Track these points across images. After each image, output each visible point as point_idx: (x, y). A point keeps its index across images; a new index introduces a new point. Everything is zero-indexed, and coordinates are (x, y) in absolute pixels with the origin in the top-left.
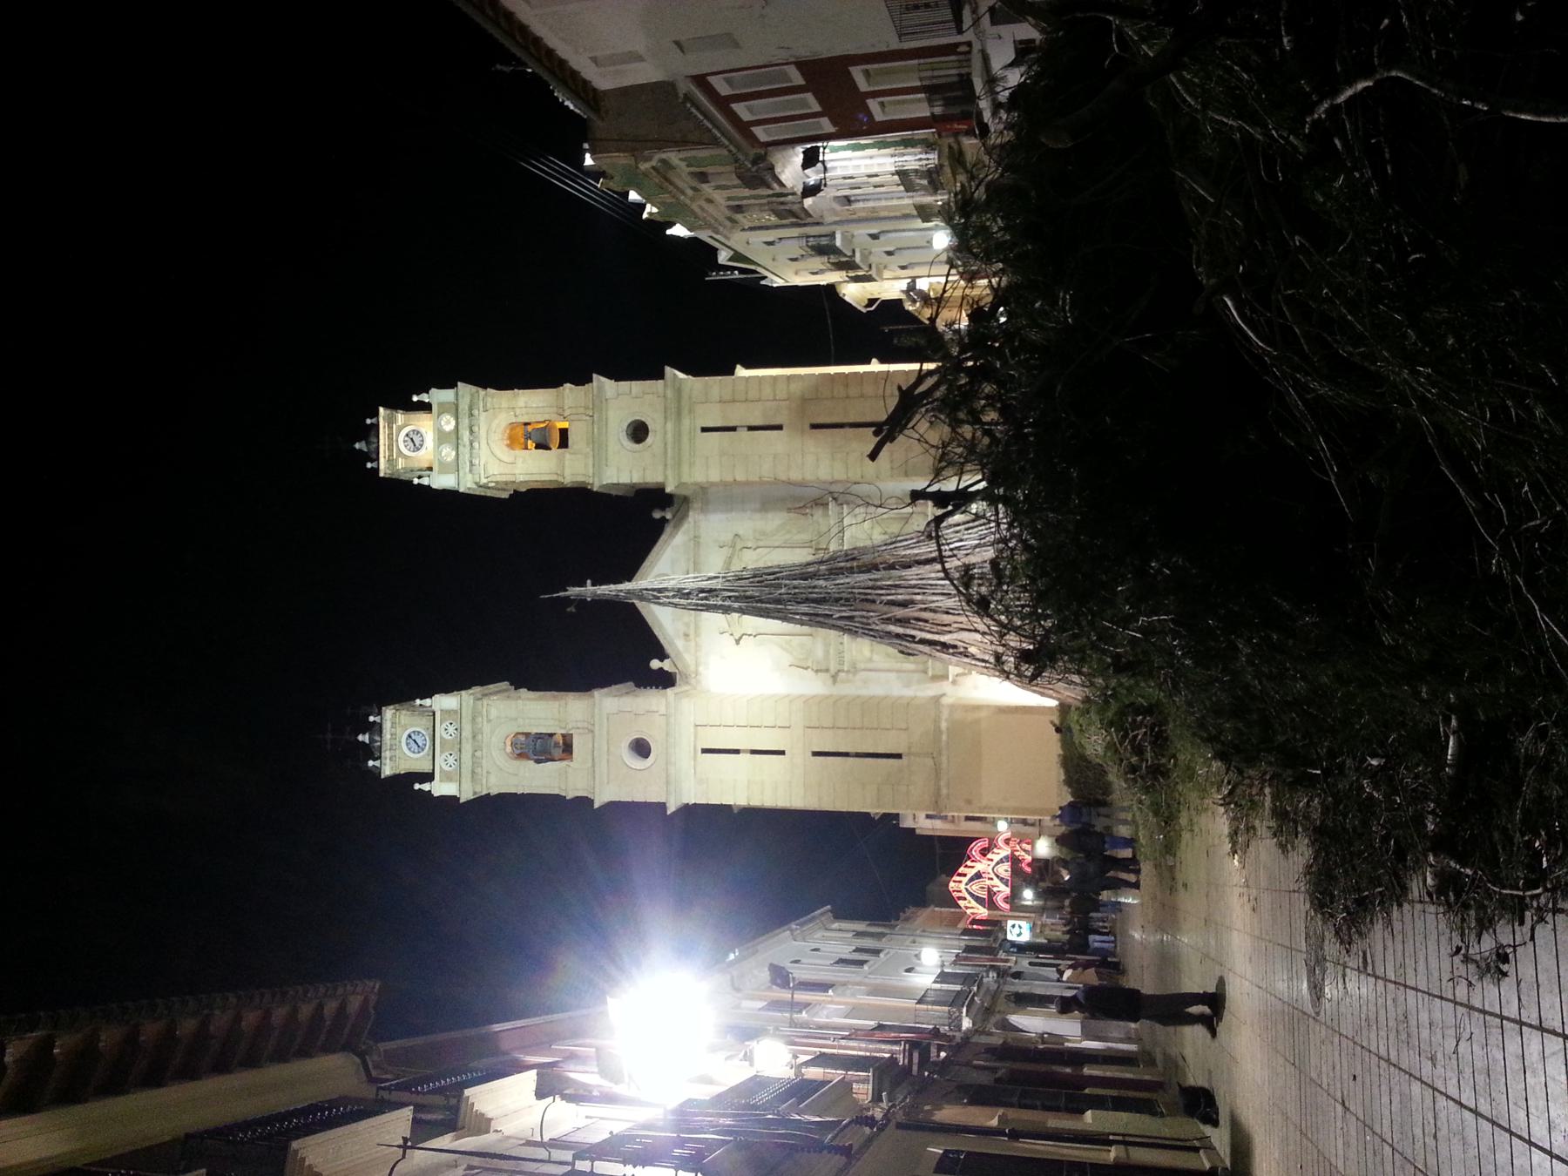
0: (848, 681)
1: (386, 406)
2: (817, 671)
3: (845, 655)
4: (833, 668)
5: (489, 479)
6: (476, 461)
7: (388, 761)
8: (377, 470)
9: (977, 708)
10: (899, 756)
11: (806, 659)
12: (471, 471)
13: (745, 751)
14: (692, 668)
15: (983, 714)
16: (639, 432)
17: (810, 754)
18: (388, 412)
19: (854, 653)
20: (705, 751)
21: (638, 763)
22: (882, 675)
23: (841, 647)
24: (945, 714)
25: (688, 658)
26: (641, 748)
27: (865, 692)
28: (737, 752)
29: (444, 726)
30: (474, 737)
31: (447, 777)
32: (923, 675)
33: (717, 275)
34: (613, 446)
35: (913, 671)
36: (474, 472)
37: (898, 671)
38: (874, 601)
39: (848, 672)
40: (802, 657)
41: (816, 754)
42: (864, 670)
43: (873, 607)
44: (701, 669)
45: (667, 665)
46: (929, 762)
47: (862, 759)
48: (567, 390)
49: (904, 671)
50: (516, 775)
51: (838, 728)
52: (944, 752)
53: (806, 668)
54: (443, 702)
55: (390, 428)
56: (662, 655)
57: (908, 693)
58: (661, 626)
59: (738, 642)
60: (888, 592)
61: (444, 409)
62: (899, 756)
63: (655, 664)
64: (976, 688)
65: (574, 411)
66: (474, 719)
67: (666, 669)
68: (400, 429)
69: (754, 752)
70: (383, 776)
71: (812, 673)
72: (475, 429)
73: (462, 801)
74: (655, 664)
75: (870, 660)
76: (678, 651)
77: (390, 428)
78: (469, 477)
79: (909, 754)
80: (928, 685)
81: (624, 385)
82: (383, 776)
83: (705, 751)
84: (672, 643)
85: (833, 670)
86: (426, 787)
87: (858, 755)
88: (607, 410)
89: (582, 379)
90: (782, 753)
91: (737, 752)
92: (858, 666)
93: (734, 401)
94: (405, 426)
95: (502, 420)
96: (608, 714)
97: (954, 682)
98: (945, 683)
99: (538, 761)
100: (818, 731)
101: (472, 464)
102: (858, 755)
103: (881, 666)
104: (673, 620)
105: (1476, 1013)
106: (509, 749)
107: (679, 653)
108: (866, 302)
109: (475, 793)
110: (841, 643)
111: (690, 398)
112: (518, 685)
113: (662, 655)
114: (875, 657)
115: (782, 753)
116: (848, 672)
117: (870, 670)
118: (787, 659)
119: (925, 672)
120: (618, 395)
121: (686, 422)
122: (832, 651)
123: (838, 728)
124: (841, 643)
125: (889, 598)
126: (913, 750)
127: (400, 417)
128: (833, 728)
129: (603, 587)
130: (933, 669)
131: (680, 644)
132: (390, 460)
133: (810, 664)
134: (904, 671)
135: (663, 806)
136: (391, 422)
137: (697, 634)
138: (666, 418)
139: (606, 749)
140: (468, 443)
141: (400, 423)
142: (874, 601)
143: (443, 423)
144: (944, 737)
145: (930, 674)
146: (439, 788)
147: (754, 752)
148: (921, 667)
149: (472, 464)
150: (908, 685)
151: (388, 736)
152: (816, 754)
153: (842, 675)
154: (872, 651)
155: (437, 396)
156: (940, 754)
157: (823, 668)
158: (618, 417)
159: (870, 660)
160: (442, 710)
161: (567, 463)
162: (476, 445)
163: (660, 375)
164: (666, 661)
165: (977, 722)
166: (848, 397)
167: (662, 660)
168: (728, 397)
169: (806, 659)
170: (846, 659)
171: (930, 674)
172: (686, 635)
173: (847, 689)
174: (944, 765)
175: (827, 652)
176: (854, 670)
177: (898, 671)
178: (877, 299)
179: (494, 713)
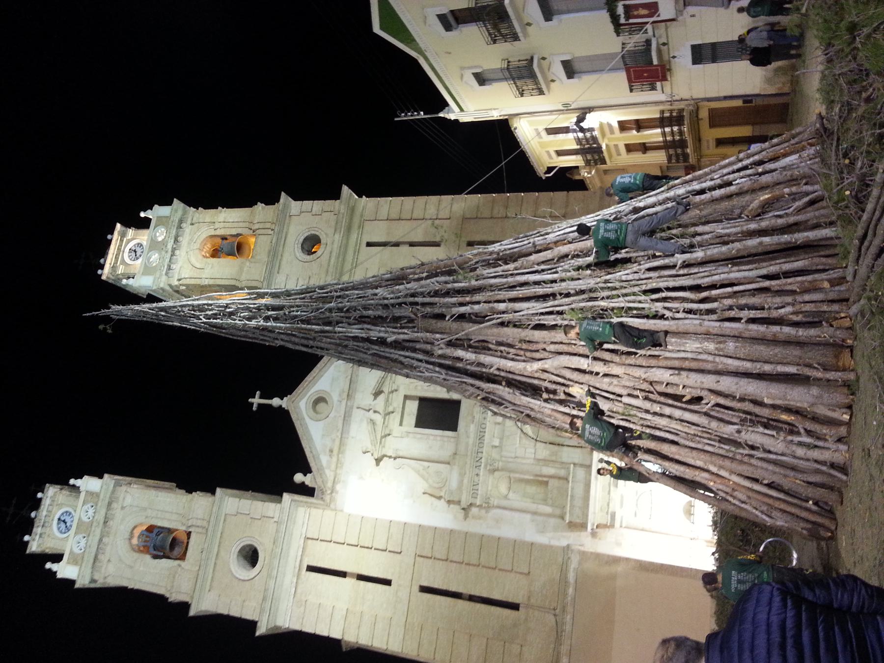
0: (480, 518)
1: (123, 224)
2: (449, 502)
3: (480, 487)
4: (465, 500)
5: (181, 282)
6: (173, 266)
7: (38, 537)
8: (101, 275)
9: (616, 560)
10: (514, 607)
11: (440, 488)
12: (167, 274)
13: (352, 575)
14: (330, 484)
15: (620, 568)
16: (311, 244)
17: (416, 588)
18: (124, 229)
19: (490, 488)
20: (311, 569)
21: (242, 572)
22: (516, 515)
23: (476, 479)
24: (574, 564)
25: (329, 474)
26: (251, 556)
27: (496, 533)
28: (342, 574)
29: (86, 507)
30: (105, 522)
31: (76, 560)
32: (559, 521)
33: (406, 115)
34: (287, 257)
35: (549, 515)
36: (170, 275)
37: (535, 513)
38: (441, 317)
39: (480, 506)
40: (437, 486)
41: (425, 589)
42: (499, 507)
43: (440, 324)
44: (338, 487)
45: (308, 480)
46: (550, 619)
47: (472, 604)
48: (260, 208)
49: (541, 514)
50: (131, 567)
51: (451, 561)
52: (569, 609)
53: (440, 498)
54: (88, 484)
55: (122, 241)
56: (307, 470)
57: (542, 539)
58: (310, 439)
59: (378, 461)
60: (461, 299)
61: (163, 221)
62: (514, 607)
63: (299, 478)
64: (618, 544)
65: (261, 226)
66: (110, 504)
67: (307, 483)
68: (129, 241)
69: (361, 578)
70: (28, 552)
71: (445, 505)
72: (180, 239)
73: (77, 586)
74: (299, 478)
75: (506, 497)
76: (322, 466)
77: (122, 241)
78: (164, 278)
79: (528, 606)
80: (564, 534)
81: (307, 204)
82: (28, 552)
83: (311, 569)
84: (317, 458)
85: (464, 504)
86: (54, 567)
87: (472, 598)
88: (288, 226)
89: (271, 200)
90: (387, 582)
91: (342, 574)
92: (491, 502)
93: (399, 219)
94: (133, 239)
95: (205, 232)
96: (226, 515)
97: (594, 534)
98: (583, 534)
99: (155, 557)
100: (430, 561)
101: (169, 268)
102: (472, 598)
103: (516, 505)
104: (323, 435)
105: (536, 613)
106: (135, 541)
107: (321, 469)
108: (546, 169)
109: (93, 581)
110: (477, 475)
111: (362, 216)
112: (180, 486)
113: (307, 470)
114: (511, 495)
115: (387, 582)
116: (480, 506)
117: (505, 508)
118: (422, 486)
119: (562, 517)
120: (301, 212)
121: (354, 236)
122: (465, 481)
123: (451, 561)
124: (477, 475)
125: (462, 309)
126: (533, 601)
127: (131, 232)
128: (447, 560)
129: (144, 306)
130: (571, 514)
131: (324, 459)
132: (114, 268)
133: (442, 494)
134: (541, 514)
135: (253, 624)
136: (123, 235)
137: (341, 451)
138: (335, 230)
139: (215, 553)
140: (170, 250)
141: (129, 237)
142: (441, 317)
143: (158, 234)
144: (571, 591)
145: (567, 519)
146: (64, 570)
147: (361, 578)
148: (558, 512)
149: (169, 268)
150: (542, 531)
151: (44, 513)
152: (425, 589)
153: (474, 510)
154: (509, 489)
155: (156, 213)
156: (564, 610)
157: (456, 499)
158: (296, 232)
159: (506, 497)
160: (87, 492)
161: (245, 269)
162: (177, 252)
163: (336, 196)
164: (308, 475)
165: (613, 577)
166: (506, 217)
167: (305, 475)
168: (394, 215)
169: (440, 488)
170: (479, 492)
171: (567, 519)
172: (331, 451)
173: (478, 526)
174: (568, 628)
175: (461, 482)
176: (487, 506)
177: (535, 513)
178: (555, 167)
179: (129, 500)
